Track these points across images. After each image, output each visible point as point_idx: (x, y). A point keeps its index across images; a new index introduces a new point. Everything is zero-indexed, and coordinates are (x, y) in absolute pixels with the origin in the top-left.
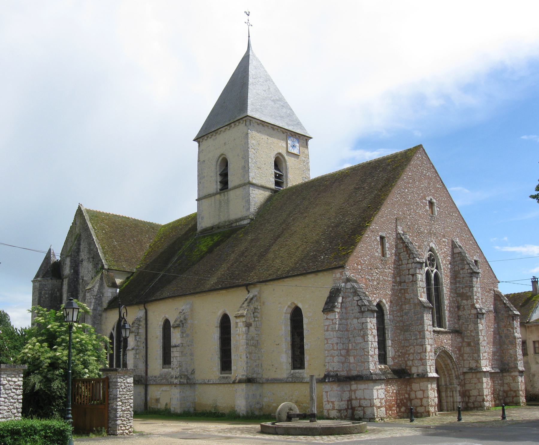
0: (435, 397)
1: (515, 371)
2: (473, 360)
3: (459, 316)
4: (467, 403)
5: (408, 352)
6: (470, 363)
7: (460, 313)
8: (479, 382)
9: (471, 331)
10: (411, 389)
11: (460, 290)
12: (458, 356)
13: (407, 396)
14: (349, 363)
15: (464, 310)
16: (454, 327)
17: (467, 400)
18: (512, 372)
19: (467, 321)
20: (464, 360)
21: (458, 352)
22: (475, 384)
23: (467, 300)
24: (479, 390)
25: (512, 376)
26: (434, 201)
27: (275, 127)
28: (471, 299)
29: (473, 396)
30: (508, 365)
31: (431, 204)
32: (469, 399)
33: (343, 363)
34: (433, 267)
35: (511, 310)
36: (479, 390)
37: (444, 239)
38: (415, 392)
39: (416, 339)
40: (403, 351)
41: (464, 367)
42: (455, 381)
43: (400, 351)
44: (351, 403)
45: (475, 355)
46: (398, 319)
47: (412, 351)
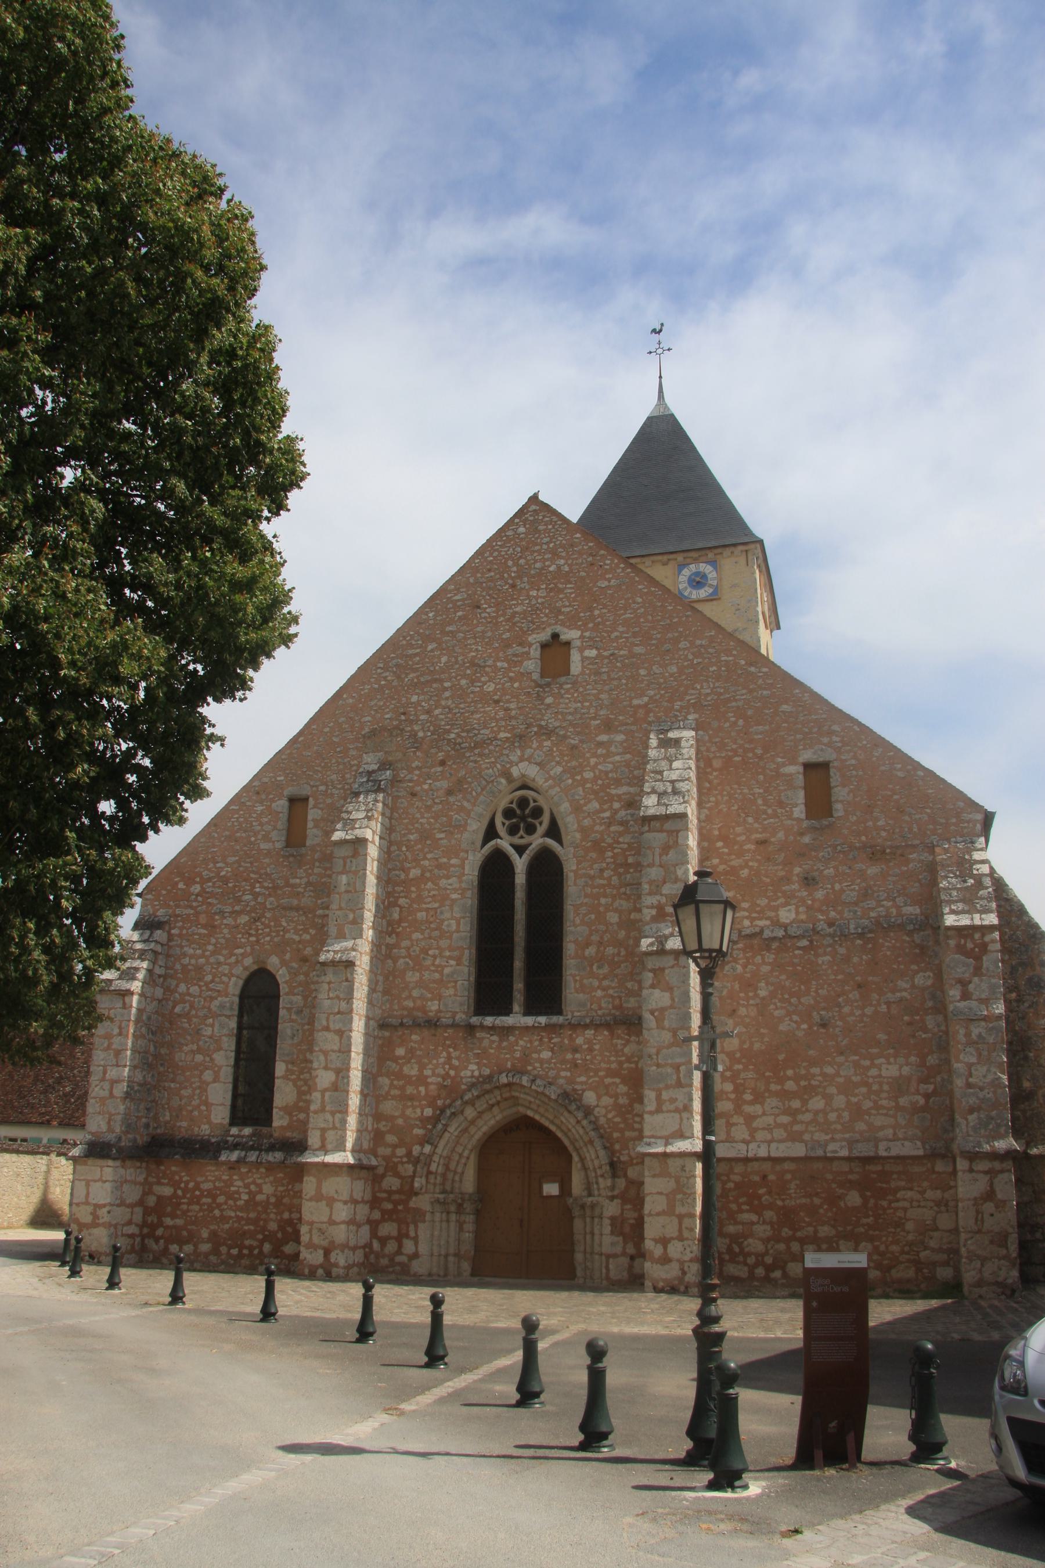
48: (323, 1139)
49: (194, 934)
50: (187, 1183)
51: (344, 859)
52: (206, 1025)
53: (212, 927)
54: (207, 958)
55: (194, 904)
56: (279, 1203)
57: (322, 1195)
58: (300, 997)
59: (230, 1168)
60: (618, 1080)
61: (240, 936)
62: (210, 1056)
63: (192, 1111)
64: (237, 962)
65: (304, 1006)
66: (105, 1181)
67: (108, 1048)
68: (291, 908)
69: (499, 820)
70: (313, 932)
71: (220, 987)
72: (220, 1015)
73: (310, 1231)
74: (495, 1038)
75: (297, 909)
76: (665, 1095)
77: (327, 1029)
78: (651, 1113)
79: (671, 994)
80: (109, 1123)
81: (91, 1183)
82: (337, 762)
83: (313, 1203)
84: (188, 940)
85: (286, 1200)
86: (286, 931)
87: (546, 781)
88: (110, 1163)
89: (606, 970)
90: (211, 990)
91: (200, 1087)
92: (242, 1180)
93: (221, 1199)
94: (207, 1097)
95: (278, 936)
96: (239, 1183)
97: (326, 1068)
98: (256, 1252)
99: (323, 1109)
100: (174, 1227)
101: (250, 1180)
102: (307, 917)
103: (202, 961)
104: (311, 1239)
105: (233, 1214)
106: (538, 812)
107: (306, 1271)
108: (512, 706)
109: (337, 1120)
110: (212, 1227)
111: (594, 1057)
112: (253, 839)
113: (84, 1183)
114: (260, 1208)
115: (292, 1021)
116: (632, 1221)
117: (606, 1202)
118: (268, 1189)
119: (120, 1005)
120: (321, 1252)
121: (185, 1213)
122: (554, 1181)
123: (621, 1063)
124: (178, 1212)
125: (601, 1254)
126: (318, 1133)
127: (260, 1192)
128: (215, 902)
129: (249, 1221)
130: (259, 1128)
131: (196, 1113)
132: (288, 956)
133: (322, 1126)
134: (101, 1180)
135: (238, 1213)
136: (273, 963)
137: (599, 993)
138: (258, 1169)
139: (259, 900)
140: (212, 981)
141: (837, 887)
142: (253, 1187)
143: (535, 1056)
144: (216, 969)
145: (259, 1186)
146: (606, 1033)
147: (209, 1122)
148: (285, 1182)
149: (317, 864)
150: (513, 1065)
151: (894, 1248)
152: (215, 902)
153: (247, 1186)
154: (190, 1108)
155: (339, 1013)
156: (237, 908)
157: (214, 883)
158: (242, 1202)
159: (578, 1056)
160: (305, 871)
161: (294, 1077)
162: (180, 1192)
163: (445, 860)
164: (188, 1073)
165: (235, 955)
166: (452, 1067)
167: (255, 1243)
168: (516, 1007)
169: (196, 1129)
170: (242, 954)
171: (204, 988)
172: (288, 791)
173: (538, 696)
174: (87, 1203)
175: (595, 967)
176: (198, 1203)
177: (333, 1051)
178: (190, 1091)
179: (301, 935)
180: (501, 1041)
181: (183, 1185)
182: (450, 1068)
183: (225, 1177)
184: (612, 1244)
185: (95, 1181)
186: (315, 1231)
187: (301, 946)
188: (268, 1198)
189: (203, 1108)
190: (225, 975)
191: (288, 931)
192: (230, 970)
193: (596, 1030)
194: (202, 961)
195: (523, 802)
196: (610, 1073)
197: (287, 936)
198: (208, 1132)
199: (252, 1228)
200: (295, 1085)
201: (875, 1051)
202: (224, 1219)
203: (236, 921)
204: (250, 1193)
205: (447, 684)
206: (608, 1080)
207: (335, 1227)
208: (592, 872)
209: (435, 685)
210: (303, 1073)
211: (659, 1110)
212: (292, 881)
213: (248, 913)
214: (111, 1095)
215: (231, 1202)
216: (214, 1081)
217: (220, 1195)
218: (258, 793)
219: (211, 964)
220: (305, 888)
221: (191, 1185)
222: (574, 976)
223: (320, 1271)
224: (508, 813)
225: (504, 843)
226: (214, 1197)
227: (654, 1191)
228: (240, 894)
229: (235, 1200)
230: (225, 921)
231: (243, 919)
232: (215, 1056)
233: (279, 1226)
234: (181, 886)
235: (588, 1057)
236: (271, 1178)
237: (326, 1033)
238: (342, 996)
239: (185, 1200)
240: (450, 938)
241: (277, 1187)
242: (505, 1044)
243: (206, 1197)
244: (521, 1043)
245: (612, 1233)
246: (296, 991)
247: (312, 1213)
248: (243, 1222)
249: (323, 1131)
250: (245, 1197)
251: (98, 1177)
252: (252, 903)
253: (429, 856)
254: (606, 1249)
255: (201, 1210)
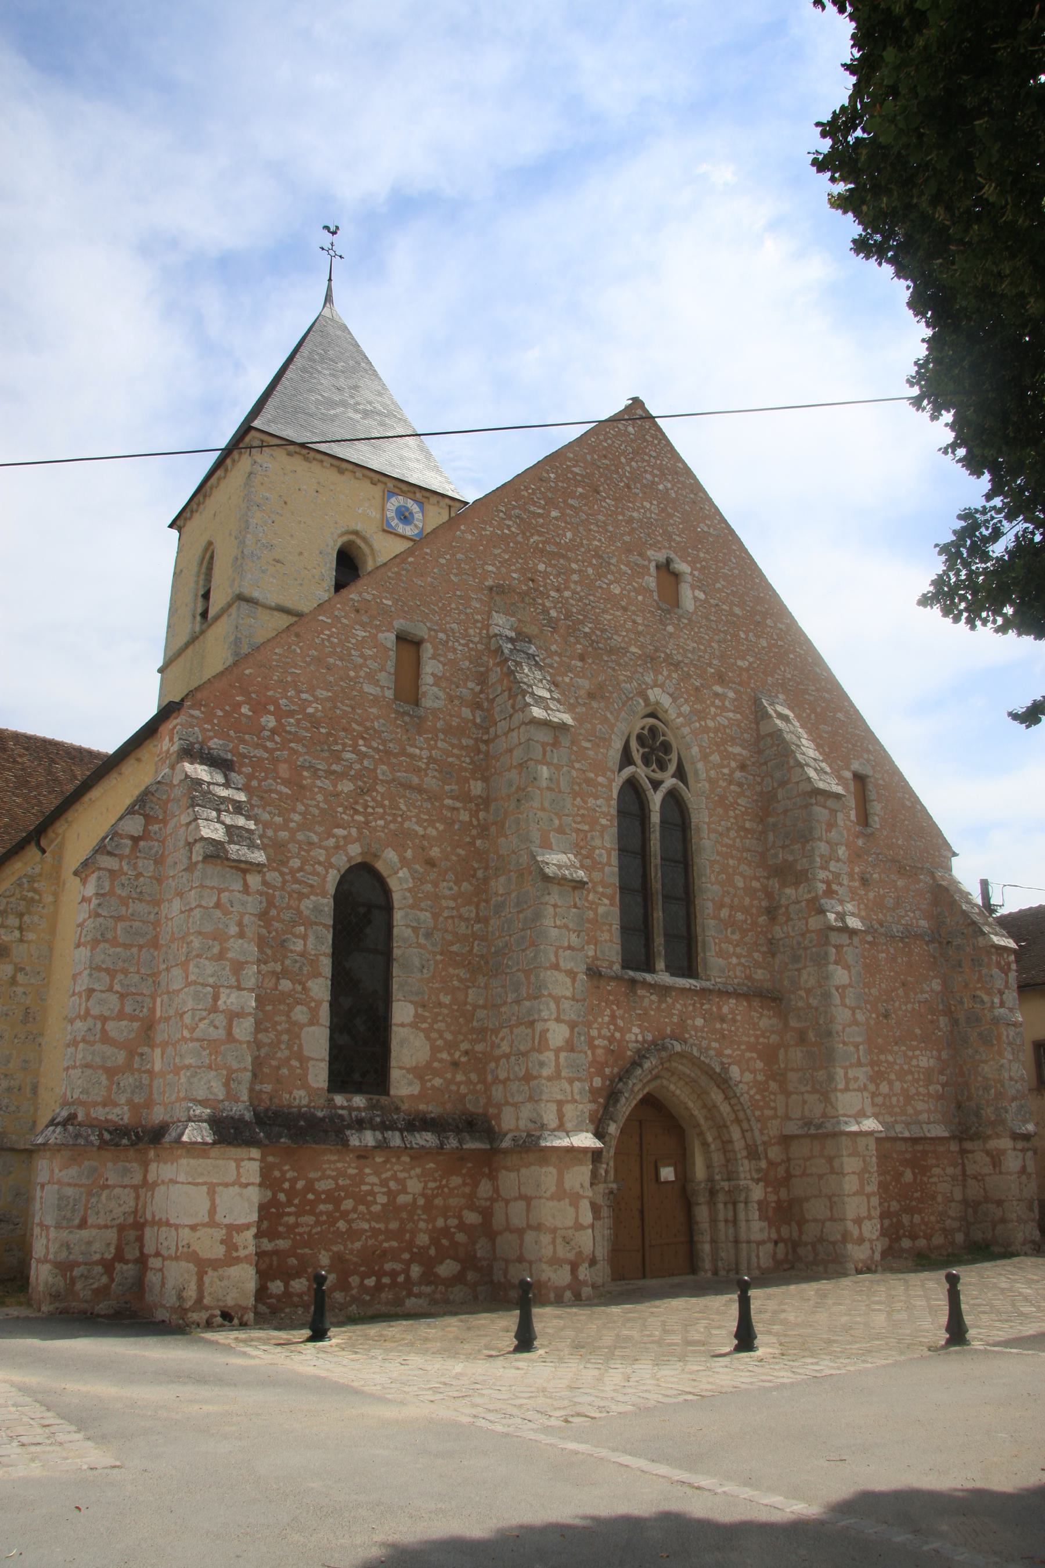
0: (579, 1227)
1: (998, 1136)
2: (814, 1091)
3: (770, 942)
4: (795, 1245)
5: (498, 1052)
6: (805, 1102)
7: (778, 932)
8: (833, 1171)
9: (808, 991)
10: (497, 1196)
11: (776, 856)
12: (761, 1078)
13: (472, 1218)
14: (150, 1072)
15: (789, 919)
16: (749, 978)
17: (795, 1235)
18: (989, 1137)
19: (796, 959)
20: (788, 1094)
21: (759, 1065)
22: (821, 1177)
23: (797, 884)
24: (830, 1198)
25: (988, 1153)
26: (682, 567)
27: (344, 465)
28: (807, 880)
29: (815, 1220)
30: (978, 1115)
31: (666, 568)
32: (801, 1233)
33: (111, 1072)
34: (662, 766)
35: (983, 934)
36: (830, 1198)
37: (718, 689)
38: (507, 1202)
39: (518, 1002)
40: (479, 1047)
41: (787, 1118)
42: (745, 1167)
43: (465, 1046)
44: (140, 1239)
45: (821, 1075)
46: (462, 929)
47: (505, 1048)
48: (561, 1116)
49: (271, 791)
50: (293, 1181)
51: (544, 745)
52: (296, 936)
53: (300, 790)
54: (293, 832)
55: (269, 744)
56: (429, 1207)
57: (565, 1191)
58: (428, 914)
59: (359, 1157)
60: (754, 1055)
61: (340, 809)
62: (303, 984)
63: (278, 1068)
64: (337, 847)
65: (435, 928)
66: (247, 1185)
67: (221, 956)
68: (409, 787)
69: (634, 744)
70: (441, 827)
71: (313, 880)
72: (316, 924)
73: (554, 1242)
74: (654, 998)
75: (419, 789)
76: (851, 1075)
77: (556, 967)
78: (842, 1091)
79: (849, 972)
80: (226, 1085)
81: (219, 1189)
82: (457, 608)
83: (555, 1203)
84: (262, 798)
85: (439, 1201)
86: (406, 818)
87: (678, 717)
88: (255, 1153)
89: (736, 937)
90: (300, 882)
91: (287, 1031)
92: (377, 1173)
93: (348, 1204)
94: (300, 1046)
95: (394, 821)
96: (374, 1179)
97: (558, 1020)
98: (401, 1279)
99: (557, 1076)
100: (276, 1252)
101: (389, 1174)
102: (432, 804)
103: (284, 835)
104: (555, 1252)
105: (366, 1226)
106: (666, 747)
107: (552, 1295)
108: (639, 620)
109: (576, 1091)
110: (335, 1249)
111: (737, 1029)
112: (352, 674)
113: (205, 1188)
114: (404, 1215)
115: (420, 946)
116: (773, 1205)
117: (752, 1185)
118: (414, 1186)
119: (238, 886)
120: (568, 1268)
121: (291, 1228)
122: (668, 1165)
123: (757, 1037)
124: (281, 1229)
125: (748, 1242)
126: (554, 1107)
127: (404, 1191)
128: (300, 749)
129: (390, 1235)
130: (376, 1097)
131: (285, 1071)
132: (409, 854)
133: (559, 1097)
134: (237, 1183)
135: (373, 1224)
136: (388, 862)
137: (734, 960)
138: (399, 1158)
139: (366, 763)
140: (301, 869)
141: (882, 892)
142: (393, 1185)
143: (689, 1022)
144: (308, 851)
145: (402, 1182)
146: (745, 1004)
147: (305, 1086)
148: (436, 1175)
149: (441, 736)
150: (672, 1031)
151: (933, 1218)
152: (300, 749)
153: (384, 1183)
154: (274, 1063)
155: (569, 947)
156: (334, 767)
157: (298, 721)
158: (379, 1208)
159: (725, 1026)
160: (427, 740)
161: (425, 1026)
162: (282, 1197)
163: (592, 775)
164: (269, 1008)
165: (334, 836)
166: (617, 1028)
167: (398, 1266)
168: (660, 965)
169: (287, 1096)
170: (345, 837)
171: (288, 878)
172: (399, 623)
173: (661, 620)
174: (212, 1223)
175: (729, 930)
176: (312, 1212)
177: (567, 998)
178: (272, 1035)
179: (425, 828)
180: (660, 1002)
181: (286, 1185)
182: (615, 1030)
183: (352, 1171)
184: (761, 1230)
185: (226, 1185)
186: (559, 1241)
187: (426, 843)
188: (415, 1200)
189: (295, 1063)
190: (320, 863)
191: (409, 818)
192: (328, 857)
193: (737, 999)
194: (284, 835)
195: (653, 730)
196: (751, 1048)
197: (406, 825)
198: (305, 1102)
199: (395, 1244)
200: (428, 1038)
201: (914, 1043)
202: (353, 1234)
203: (335, 786)
204: (389, 1193)
205: (574, 566)
206: (748, 1055)
207: (582, 1232)
208: (720, 829)
209: (562, 561)
210: (437, 1022)
211: (847, 1089)
212: (411, 750)
213: (354, 779)
214: (230, 1037)
215: (362, 1208)
216: (311, 1023)
217: (346, 1197)
218: (357, 611)
219: (299, 842)
220: (427, 764)
221: (300, 1184)
222: (714, 938)
223: (568, 1294)
224: (640, 738)
225: (641, 771)
226: (337, 1202)
227: (850, 1171)
228: (339, 747)
229: (368, 1205)
230: (318, 783)
231: (346, 786)
232: (310, 984)
233: (431, 1239)
234: (245, 710)
235: (733, 1028)
236: (418, 1170)
237: (556, 973)
238: (571, 926)
239: (292, 1209)
240: (602, 870)
241: (426, 1183)
242: (664, 1006)
243: (325, 1202)
244: (678, 1006)
245: (760, 1219)
246: (423, 905)
247: (554, 1217)
248: (381, 1237)
249: (560, 1104)
250: (382, 1199)
251: (231, 1177)
252: (357, 766)
253: (577, 765)
254: (756, 1236)
255: (318, 1223)
